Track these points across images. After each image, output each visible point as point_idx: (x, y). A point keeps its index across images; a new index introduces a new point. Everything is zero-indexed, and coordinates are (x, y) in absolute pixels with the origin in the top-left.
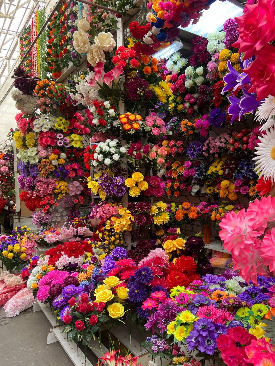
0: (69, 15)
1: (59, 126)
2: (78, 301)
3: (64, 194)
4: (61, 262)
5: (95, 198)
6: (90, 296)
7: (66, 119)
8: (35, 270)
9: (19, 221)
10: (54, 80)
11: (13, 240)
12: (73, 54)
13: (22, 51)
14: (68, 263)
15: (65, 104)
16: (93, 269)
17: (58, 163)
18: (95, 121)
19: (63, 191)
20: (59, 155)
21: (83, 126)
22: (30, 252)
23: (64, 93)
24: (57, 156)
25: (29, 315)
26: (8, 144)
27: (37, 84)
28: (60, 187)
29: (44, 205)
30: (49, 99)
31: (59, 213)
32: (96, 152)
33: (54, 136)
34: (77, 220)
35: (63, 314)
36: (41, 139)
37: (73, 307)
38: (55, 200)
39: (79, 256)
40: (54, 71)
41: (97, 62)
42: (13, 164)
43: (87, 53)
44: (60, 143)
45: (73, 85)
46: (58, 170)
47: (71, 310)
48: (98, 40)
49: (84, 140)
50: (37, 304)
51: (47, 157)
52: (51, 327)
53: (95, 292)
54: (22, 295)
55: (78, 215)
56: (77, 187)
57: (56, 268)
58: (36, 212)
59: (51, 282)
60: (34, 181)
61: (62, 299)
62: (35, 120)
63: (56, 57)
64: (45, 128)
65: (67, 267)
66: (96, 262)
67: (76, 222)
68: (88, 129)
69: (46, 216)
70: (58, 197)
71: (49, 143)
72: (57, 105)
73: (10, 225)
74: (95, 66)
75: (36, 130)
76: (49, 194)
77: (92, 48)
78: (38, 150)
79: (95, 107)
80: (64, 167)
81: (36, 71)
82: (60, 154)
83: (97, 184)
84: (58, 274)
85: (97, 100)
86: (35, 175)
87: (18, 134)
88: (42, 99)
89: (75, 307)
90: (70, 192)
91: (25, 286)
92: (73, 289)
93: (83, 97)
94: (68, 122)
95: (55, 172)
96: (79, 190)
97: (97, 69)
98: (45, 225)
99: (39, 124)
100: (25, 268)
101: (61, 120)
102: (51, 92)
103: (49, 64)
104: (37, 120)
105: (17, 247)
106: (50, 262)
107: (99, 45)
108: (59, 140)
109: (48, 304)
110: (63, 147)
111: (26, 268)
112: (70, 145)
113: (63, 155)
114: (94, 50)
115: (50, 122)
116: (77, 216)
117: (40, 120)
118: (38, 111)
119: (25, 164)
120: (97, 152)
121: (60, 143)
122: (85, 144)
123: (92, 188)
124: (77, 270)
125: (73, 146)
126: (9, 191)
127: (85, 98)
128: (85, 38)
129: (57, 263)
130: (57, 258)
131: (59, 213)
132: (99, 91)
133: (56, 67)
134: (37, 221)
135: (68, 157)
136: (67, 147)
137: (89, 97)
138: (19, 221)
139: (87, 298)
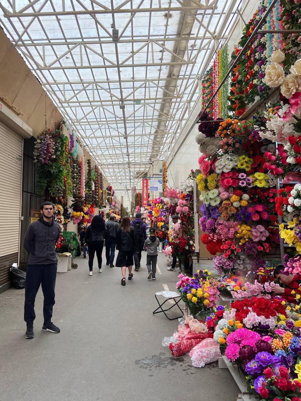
0: (256, 47)
1: (242, 165)
2: (275, 374)
3: (247, 240)
4: (249, 320)
5: (284, 247)
6: (289, 371)
7: (249, 157)
8: (221, 322)
9: (198, 262)
10: (237, 118)
11: (196, 283)
12: (260, 88)
13: (204, 93)
14: (257, 323)
15: (249, 141)
16: (291, 338)
17: (240, 205)
18: (290, 160)
19: (245, 236)
20: (241, 196)
21: (274, 167)
22: (212, 299)
23: (248, 129)
24: (239, 198)
25: (214, 370)
26: (189, 185)
27: (220, 125)
28: (242, 231)
29: (226, 250)
30: (232, 138)
31: (241, 260)
32: (290, 196)
33: (236, 176)
34: (263, 271)
35: (257, 384)
36: (223, 180)
37: (269, 379)
38: (237, 245)
39: (270, 317)
40: (238, 108)
41: (293, 93)
42: (192, 204)
43: (281, 85)
44: (243, 183)
45: (262, 122)
46: (239, 213)
47: (267, 382)
48: (295, 69)
49: (269, 178)
50: (223, 361)
51: (228, 198)
52: (240, 392)
53: (296, 367)
54: (206, 346)
55: (263, 265)
56: (261, 233)
57: (244, 326)
58: (217, 257)
59: (241, 341)
60: (215, 224)
61: (255, 366)
62: (216, 161)
63: (240, 94)
64: (227, 169)
65: (257, 327)
66: (292, 329)
67: (261, 273)
68: (280, 169)
69: (228, 262)
70: (240, 242)
71: (231, 184)
72: (240, 143)
73: (190, 265)
74: (291, 97)
75: (218, 171)
76: (229, 238)
77: (288, 79)
78: (219, 192)
79: (291, 144)
80: (247, 209)
81: (217, 110)
82: (242, 195)
83: (292, 233)
84: (248, 333)
85: (293, 136)
86: (216, 217)
87: (201, 177)
88: (225, 140)
89: (272, 380)
90: (253, 238)
91: (211, 335)
92: (269, 358)
93: (274, 134)
94: (251, 160)
95: (237, 214)
96: (264, 235)
97: (293, 101)
98: (226, 271)
99: (221, 165)
100: (210, 317)
101: (244, 159)
102: (234, 131)
103: (233, 102)
104: (218, 161)
105: (200, 292)
106: (237, 317)
107: (297, 74)
108: (241, 180)
109: (236, 365)
110: (246, 187)
111: (211, 318)
112: (253, 184)
113: (246, 196)
114: (290, 80)
115: (232, 162)
116: (262, 266)
117: (222, 161)
118: (221, 152)
119: (207, 206)
120: (293, 196)
121: (243, 183)
122: (271, 183)
123: (286, 238)
124: (269, 334)
125: (256, 186)
126: (189, 231)
127: (276, 135)
128: (279, 70)
129: (245, 320)
130: (245, 314)
131: (241, 260)
132: (295, 125)
133: (240, 104)
134: (219, 267)
135: (251, 198)
136: (249, 187)
137: (282, 132)
138: (198, 262)
139: (287, 373)
